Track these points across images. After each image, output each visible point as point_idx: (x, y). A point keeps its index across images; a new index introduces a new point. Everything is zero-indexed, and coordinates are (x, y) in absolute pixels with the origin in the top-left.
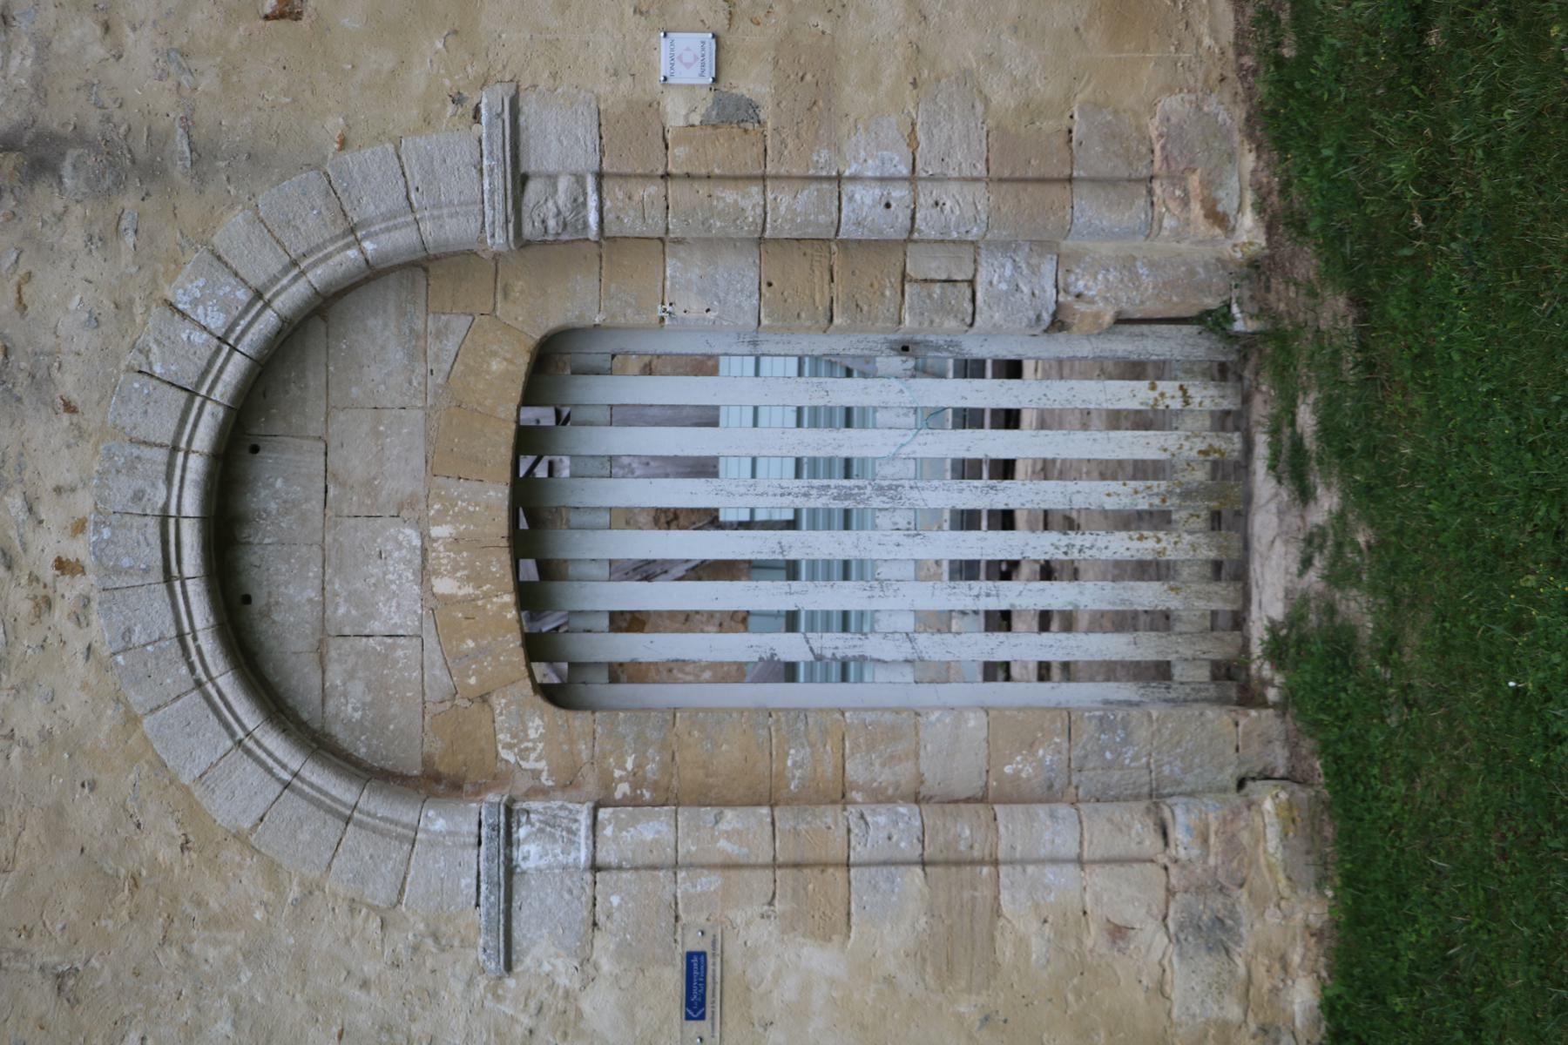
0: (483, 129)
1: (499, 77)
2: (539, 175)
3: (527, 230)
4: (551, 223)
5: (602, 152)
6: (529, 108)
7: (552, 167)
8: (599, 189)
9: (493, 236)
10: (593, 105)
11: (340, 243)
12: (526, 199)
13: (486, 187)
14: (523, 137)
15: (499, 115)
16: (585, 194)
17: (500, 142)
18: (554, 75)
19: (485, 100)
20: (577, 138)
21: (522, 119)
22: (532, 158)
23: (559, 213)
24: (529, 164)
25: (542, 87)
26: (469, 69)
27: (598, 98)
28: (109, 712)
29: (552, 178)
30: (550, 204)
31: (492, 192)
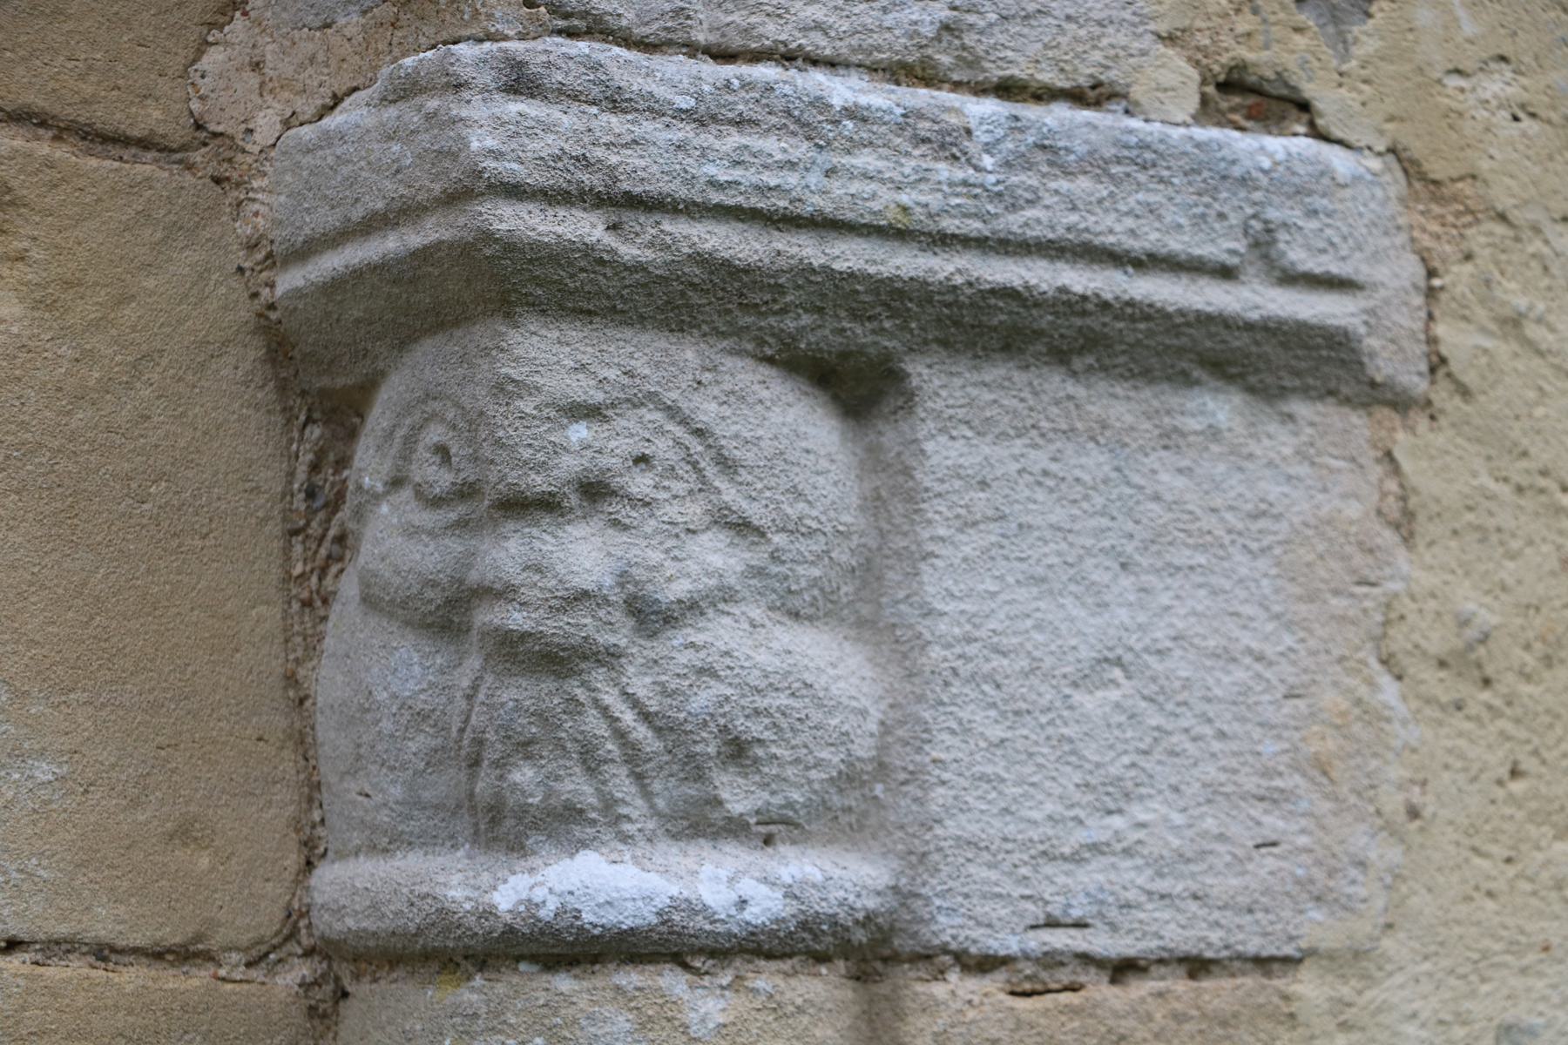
0: (1170, 117)
1: (1458, 277)
2: (893, 490)
3: (551, 357)
4: (583, 553)
5: (1035, 976)
6: (1274, 466)
7: (963, 588)
8: (802, 943)
9: (520, 82)
10: (1315, 926)
11: (259, 196)
12: (745, 375)
13: (842, 90)
14: (1118, 405)
15: (1263, 244)
16: (768, 830)
17: (1111, 229)
18: (1468, 661)
19: (1340, 161)
20: (1116, 795)
21: (1219, 408)
22: (1002, 457)
23: (651, 616)
24: (965, 425)
25: (1407, 570)
26: (1495, 86)
27: (1353, 960)
28: (44, 771)
29: (864, 593)
30: (716, 556)
31: (806, 121)
